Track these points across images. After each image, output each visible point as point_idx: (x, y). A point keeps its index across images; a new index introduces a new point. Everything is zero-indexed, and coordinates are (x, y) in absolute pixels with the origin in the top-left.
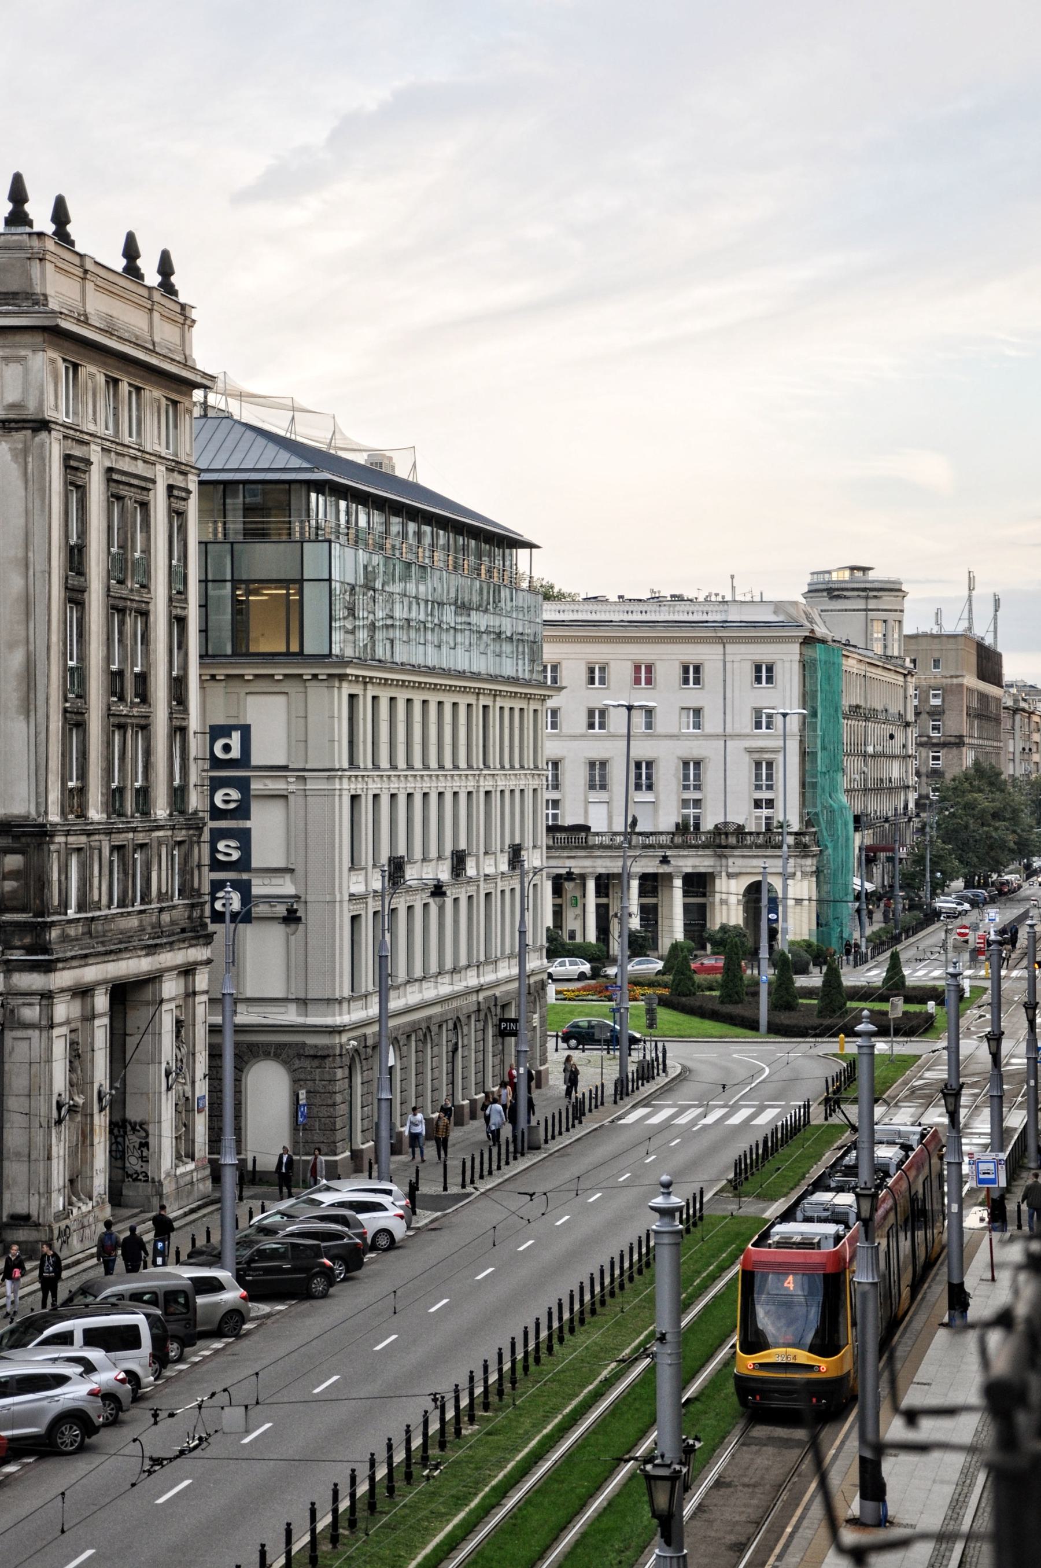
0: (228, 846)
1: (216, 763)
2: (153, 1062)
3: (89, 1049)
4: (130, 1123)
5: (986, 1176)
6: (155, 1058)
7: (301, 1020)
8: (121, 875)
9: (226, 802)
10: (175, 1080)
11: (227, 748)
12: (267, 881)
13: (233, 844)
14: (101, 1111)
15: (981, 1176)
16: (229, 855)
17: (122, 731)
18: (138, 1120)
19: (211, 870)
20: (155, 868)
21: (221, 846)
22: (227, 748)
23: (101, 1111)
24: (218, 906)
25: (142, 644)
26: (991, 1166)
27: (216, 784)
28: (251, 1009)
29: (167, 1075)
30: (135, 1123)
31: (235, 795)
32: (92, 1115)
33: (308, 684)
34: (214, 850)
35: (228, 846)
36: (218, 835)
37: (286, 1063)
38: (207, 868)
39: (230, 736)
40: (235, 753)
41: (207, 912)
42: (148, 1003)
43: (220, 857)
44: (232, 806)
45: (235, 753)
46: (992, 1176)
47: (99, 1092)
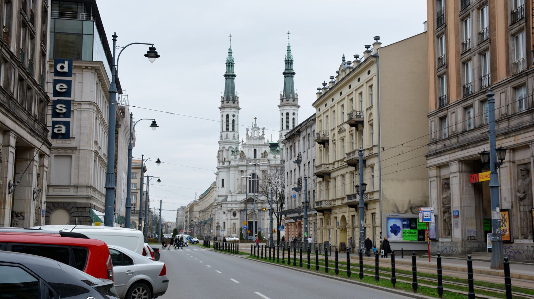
0: (61, 107)
1: (57, 73)
2: (28, 186)
3: (6, 160)
4: (15, 213)
5: (427, 217)
6: (30, 184)
7: (75, 194)
8: (21, 93)
9: (61, 89)
10: (37, 196)
11: (62, 67)
12: (64, 142)
13: (64, 106)
14: (9, 193)
15: (425, 218)
16: (62, 110)
17: (25, 29)
18: (19, 211)
19: (53, 117)
20: (34, 101)
21: (58, 106)
22: (62, 67)
23: (9, 193)
24: (56, 131)
25: (32, 3)
26: (429, 213)
27: (56, 82)
28: (55, 190)
29: (34, 194)
30: (18, 213)
31: (65, 86)
32: (5, 194)
33: (84, 70)
34: (54, 108)
35: (61, 107)
36: (55, 103)
37: (68, 211)
38: (51, 116)
39: (64, 63)
40: (66, 70)
41: (50, 134)
42: (27, 160)
43: (58, 111)
44: (64, 90)
45: (66, 70)
46: (429, 217)
47: (9, 184)
